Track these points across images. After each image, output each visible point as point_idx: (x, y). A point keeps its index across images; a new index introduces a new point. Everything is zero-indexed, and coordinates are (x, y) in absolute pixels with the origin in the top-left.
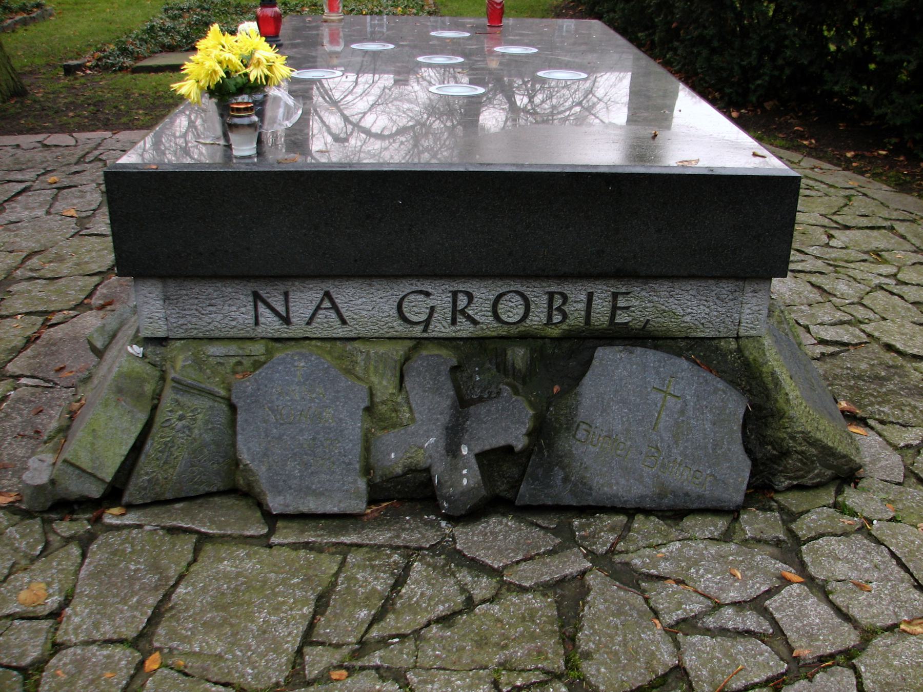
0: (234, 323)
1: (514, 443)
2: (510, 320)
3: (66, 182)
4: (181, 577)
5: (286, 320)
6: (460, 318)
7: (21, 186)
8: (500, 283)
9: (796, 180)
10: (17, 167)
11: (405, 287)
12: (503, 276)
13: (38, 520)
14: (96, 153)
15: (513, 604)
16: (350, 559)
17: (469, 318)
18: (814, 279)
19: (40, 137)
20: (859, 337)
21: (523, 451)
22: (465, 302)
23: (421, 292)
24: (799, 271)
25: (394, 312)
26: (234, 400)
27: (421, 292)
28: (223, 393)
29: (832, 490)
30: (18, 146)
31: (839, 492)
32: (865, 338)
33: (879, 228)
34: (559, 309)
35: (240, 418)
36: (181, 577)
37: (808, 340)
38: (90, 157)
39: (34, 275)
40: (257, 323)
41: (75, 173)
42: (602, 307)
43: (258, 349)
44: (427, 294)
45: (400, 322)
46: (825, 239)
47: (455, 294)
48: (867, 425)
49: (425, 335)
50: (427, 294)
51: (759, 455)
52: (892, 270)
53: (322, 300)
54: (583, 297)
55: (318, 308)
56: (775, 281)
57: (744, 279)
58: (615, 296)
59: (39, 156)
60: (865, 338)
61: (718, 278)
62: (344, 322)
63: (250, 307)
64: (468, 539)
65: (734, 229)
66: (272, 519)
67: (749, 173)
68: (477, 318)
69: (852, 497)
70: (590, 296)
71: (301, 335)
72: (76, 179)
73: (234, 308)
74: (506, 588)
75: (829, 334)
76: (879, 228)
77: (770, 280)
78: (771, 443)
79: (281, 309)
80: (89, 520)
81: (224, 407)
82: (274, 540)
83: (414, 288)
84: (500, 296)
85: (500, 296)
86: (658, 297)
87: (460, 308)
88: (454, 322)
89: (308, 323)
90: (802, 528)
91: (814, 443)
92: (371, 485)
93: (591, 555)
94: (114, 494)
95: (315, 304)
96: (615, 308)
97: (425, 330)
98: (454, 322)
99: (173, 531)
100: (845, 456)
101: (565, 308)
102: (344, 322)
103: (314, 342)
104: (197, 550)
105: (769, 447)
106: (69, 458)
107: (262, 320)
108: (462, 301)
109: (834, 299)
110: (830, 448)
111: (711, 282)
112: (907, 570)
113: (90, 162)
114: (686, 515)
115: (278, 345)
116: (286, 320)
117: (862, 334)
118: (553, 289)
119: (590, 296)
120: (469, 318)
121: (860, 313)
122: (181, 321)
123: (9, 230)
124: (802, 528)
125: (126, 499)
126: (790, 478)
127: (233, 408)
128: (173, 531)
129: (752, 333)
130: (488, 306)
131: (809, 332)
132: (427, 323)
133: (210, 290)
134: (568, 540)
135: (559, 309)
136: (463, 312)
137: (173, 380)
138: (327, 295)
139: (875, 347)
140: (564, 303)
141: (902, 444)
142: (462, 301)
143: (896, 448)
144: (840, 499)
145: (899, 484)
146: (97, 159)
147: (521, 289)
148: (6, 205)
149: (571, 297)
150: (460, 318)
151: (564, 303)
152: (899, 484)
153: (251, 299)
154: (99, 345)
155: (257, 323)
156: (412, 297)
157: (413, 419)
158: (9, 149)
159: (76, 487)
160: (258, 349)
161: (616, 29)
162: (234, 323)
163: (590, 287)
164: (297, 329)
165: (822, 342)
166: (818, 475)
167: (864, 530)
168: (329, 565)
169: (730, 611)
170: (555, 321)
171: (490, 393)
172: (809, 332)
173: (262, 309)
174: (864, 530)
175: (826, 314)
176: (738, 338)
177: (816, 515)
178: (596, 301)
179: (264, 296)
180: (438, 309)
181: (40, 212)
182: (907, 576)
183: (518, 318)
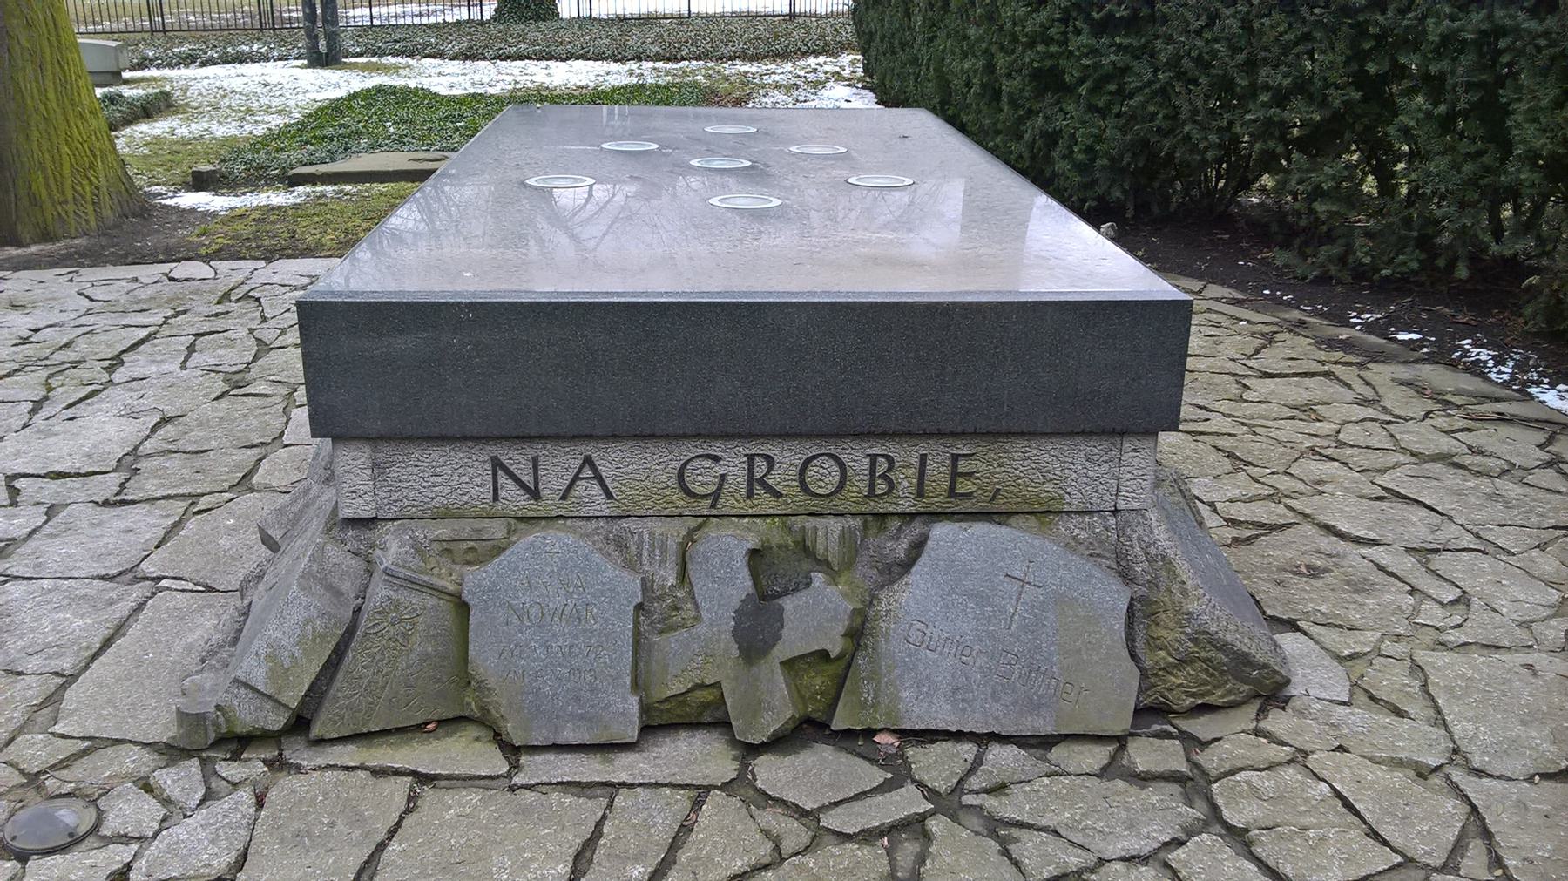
0: (466, 498)
1: (829, 647)
2: (821, 491)
3: (207, 327)
4: (392, 833)
5: (535, 494)
6: (758, 490)
7: (143, 333)
8: (809, 444)
9: (1190, 303)
10: (136, 307)
11: (691, 449)
13: (195, 762)
14: (247, 288)
15: (833, 856)
16: (619, 801)
18: (1221, 443)
19: (166, 267)
20: (1285, 516)
21: (839, 657)
22: (765, 468)
23: (708, 456)
24: (1201, 433)
25: (673, 482)
26: (466, 597)
27: (708, 456)
28: (451, 588)
29: (1252, 709)
30: (136, 280)
31: (1262, 713)
32: (1291, 517)
33: (1313, 375)
35: (474, 618)
36: (392, 833)
37: (1212, 521)
38: (239, 293)
39: (170, 447)
40: (496, 498)
41: (217, 315)
42: (938, 470)
43: (497, 529)
44: (716, 459)
45: (682, 495)
46: (1235, 390)
47: (751, 458)
48: (1298, 629)
49: (713, 512)
50: (716, 459)
51: (1148, 664)
52: (1326, 427)
54: (915, 461)
55: (576, 478)
56: (1162, 436)
57: (1122, 434)
58: (955, 458)
59: (169, 289)
60: (1291, 517)
61: (1086, 434)
62: (609, 495)
63: (488, 477)
64: (771, 772)
65: (1107, 375)
66: (512, 751)
68: (779, 488)
69: (1277, 722)
70: (923, 458)
71: (553, 514)
72: (218, 324)
73: (466, 479)
74: (820, 836)
75: (1241, 512)
76: (1313, 375)
78: (1165, 648)
79: (528, 479)
80: (264, 761)
81: (445, 606)
82: (518, 780)
83: (700, 451)
86: (1010, 459)
87: (757, 476)
89: (564, 498)
90: (1210, 760)
91: (1223, 647)
92: (645, 709)
93: (931, 793)
94: (299, 724)
95: (572, 473)
96: (955, 475)
97: (713, 506)
98: (750, 495)
99: (379, 772)
100: (1265, 666)
101: (891, 475)
102: (609, 495)
103: (569, 522)
104: (412, 798)
105: (1163, 653)
106: (242, 676)
107: (502, 494)
108: (761, 467)
109: (1250, 469)
110: (1246, 655)
111: (1078, 439)
112: (1357, 813)
113: (238, 300)
114: (1056, 743)
115: (521, 526)
116: (535, 494)
117: (1290, 514)
118: (876, 451)
119: (923, 458)
121: (1284, 483)
122: (395, 496)
123: (130, 390)
124: (1210, 760)
125: (316, 731)
126: (1193, 695)
127: (463, 608)
128: (379, 772)
129: (1136, 505)
130: (793, 474)
131: (1215, 511)
132: (716, 496)
133: (435, 455)
134: (899, 775)
135: (883, 476)
136: (762, 482)
137: (385, 572)
138: (588, 461)
139: (1310, 530)
140: (890, 469)
141: (1346, 652)
142: (761, 467)
143: (1340, 659)
144: (1262, 724)
145: (1344, 703)
146: (246, 296)
148: (125, 358)
150: (758, 490)
151: (890, 469)
152: (1344, 703)
153: (488, 466)
154: (276, 534)
155: (496, 498)
156: (696, 463)
157: (698, 618)
158: (123, 283)
159: (249, 715)
160: (497, 529)
162: (466, 498)
163: (923, 447)
164: (550, 503)
165: (1231, 522)
166: (1230, 692)
167: (1300, 757)
168: (596, 807)
169: (1119, 866)
170: (879, 492)
171: (797, 584)
172: (1215, 511)
173: (503, 479)
174: (1300, 757)
175: (1240, 485)
176: (1115, 512)
177: (1231, 739)
178: (931, 466)
179: (506, 462)
180: (730, 479)
181: (174, 367)
182: (1356, 820)
183: (831, 489)
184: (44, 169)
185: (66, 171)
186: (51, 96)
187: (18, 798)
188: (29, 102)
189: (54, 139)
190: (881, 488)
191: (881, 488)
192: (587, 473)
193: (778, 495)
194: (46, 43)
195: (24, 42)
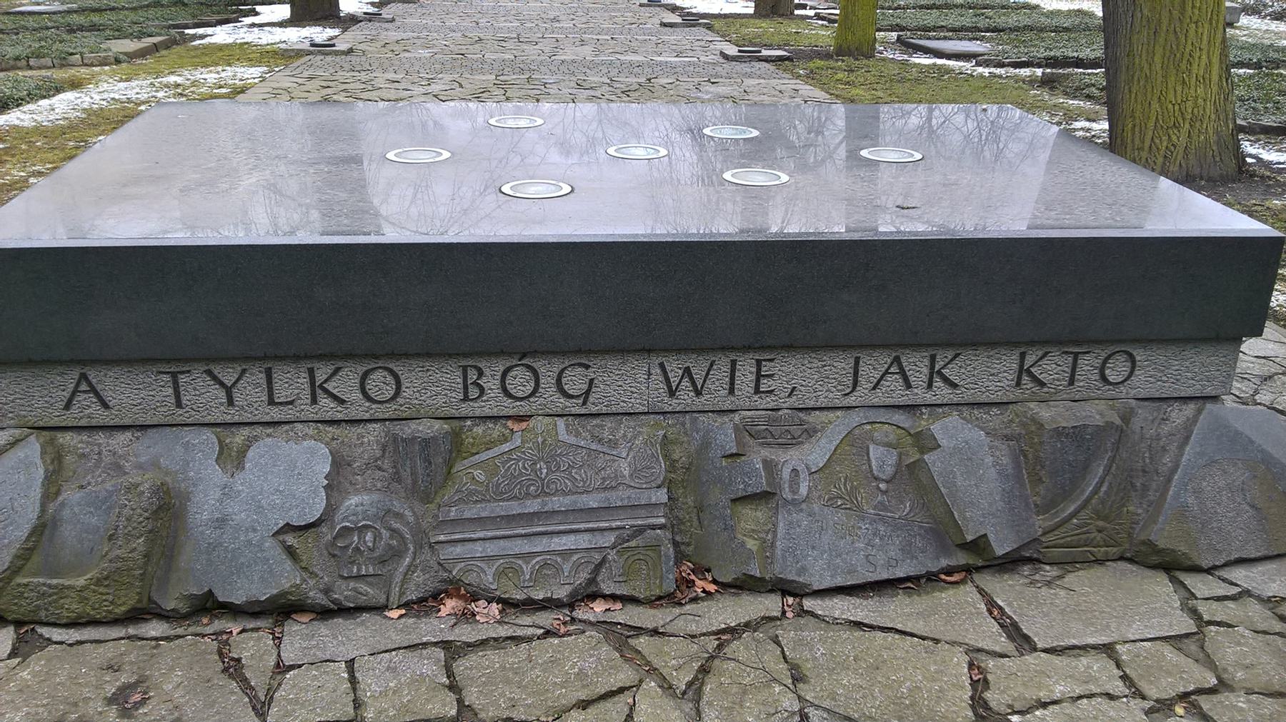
6: (1025, 378)
12: (564, 353)
17: (946, 380)
23: (580, 365)
34: (475, 383)
47: (465, 369)
50: (587, 367)
53: (78, 385)
55: (887, 372)
58: (759, 362)
67: (551, 240)
77: (1238, 341)
84: (563, 371)
85: (563, 371)
88: (314, 401)
96: (759, 376)
98: (314, 401)
108: (472, 375)
112: (912, 635)
120: (946, 380)
135: (475, 383)
136: (939, 373)
142: (472, 375)
147: (390, 366)
149: (487, 372)
161: (1181, 183)
184: (1132, 116)
185: (1151, 124)
186: (1157, 59)
187: (609, 614)
188: (1137, 61)
189: (1149, 96)
190: (474, 392)
191: (474, 392)
192: (84, 387)
193: (954, 386)
194: (1165, 14)
195: (1146, 12)
